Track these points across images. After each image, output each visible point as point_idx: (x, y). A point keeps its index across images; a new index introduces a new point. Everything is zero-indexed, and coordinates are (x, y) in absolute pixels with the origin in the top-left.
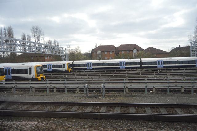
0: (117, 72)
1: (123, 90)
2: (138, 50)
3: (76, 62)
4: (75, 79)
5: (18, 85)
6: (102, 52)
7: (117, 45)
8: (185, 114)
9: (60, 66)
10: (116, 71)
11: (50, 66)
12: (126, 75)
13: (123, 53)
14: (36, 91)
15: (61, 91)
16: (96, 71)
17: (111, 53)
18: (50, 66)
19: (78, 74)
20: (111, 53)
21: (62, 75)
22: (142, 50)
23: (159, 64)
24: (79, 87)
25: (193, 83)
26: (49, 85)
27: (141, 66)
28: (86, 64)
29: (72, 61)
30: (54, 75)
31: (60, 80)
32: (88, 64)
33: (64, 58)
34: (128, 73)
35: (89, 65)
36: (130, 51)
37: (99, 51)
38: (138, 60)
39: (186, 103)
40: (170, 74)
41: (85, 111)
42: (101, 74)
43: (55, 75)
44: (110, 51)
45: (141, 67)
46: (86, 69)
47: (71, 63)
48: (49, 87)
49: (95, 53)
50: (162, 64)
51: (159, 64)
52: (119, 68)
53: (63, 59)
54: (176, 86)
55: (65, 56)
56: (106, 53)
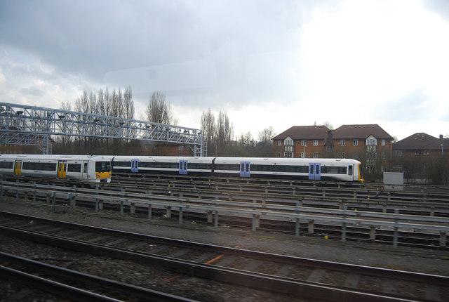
0: (146, 179)
1: (248, 221)
2: (379, 140)
3: (220, 160)
4: (144, 191)
5: (38, 191)
6: (295, 140)
7: (335, 125)
8: (321, 281)
9: (342, 170)
10: (339, 187)
11: (183, 164)
12: (353, 197)
13: (343, 144)
14: (105, 208)
15: (90, 207)
16: (146, 177)
17: (316, 144)
18: (183, 164)
19: (375, 194)
20: (316, 144)
21: (239, 187)
22: (389, 139)
23: (312, 172)
24: (172, 209)
25: (397, 220)
26: (123, 199)
27: (213, 171)
28: (308, 167)
29: (111, 157)
30: (330, 191)
31: (200, 196)
32: (243, 165)
33: (197, 151)
34: (269, 188)
35: (315, 170)
36: (360, 140)
37: (289, 139)
38: (208, 160)
39: (440, 274)
40: (243, 190)
41: (307, 279)
42: (327, 191)
43: (233, 186)
44: (312, 140)
45: (213, 174)
46: (129, 171)
47: (110, 160)
48: (124, 204)
49: (280, 144)
50: (317, 173)
51: (312, 172)
52: (238, 175)
53: (195, 152)
54: (187, 207)
55: (199, 146)
56: (303, 144)
